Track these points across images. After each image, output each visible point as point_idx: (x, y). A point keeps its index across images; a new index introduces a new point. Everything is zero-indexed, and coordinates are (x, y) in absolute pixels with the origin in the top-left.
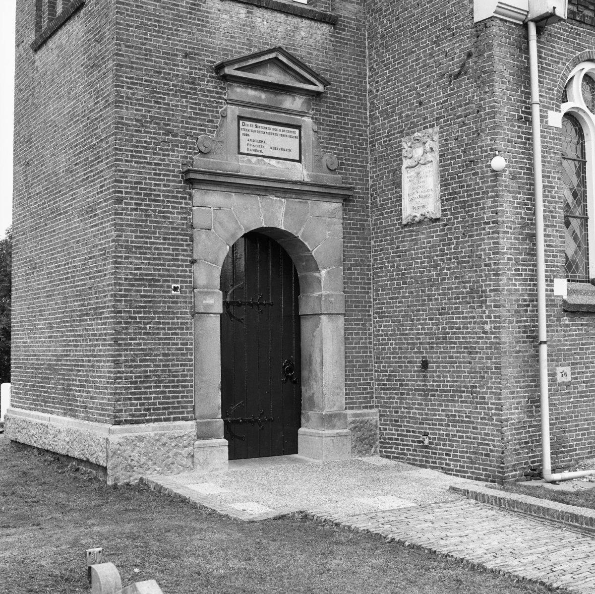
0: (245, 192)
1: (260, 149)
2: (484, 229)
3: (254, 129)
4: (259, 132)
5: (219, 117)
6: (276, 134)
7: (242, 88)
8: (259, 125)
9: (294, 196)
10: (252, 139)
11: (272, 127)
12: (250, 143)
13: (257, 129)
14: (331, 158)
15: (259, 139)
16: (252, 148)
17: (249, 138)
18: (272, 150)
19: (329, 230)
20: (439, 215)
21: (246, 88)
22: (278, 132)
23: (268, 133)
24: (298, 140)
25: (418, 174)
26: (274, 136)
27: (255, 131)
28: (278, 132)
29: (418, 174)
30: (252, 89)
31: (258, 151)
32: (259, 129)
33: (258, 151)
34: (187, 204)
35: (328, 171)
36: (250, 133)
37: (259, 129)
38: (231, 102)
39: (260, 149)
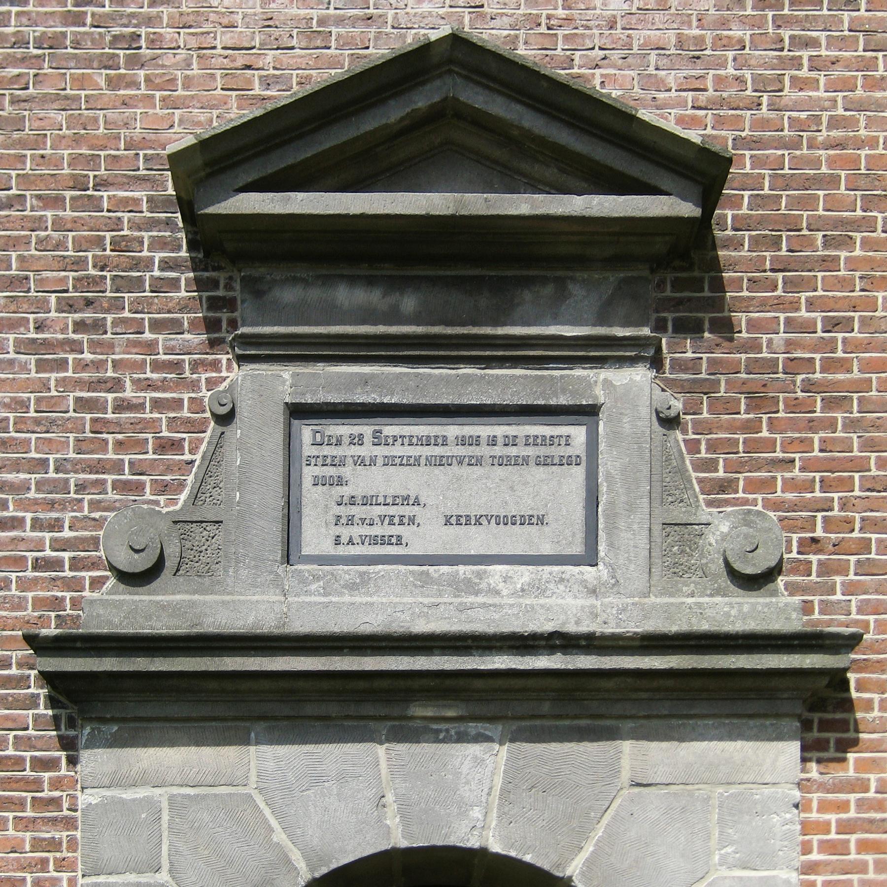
0: (310, 709)
1: (396, 530)
2: (116, 385)
3: (366, 450)
4: (389, 461)
5: (205, 421)
6: (477, 462)
7: (305, 282)
8: (391, 429)
9: (546, 707)
10: (359, 493)
11: (453, 430)
12: (342, 511)
13: (381, 451)
14: (748, 524)
15: (391, 492)
16: (357, 531)
17: (346, 491)
18: (453, 530)
19: (724, 842)
20: (303, 426)
21: (327, 280)
22: (484, 450)
23: (440, 462)
24: (579, 473)
25: (223, 433)
26: (465, 470)
27: (373, 461)
28: (484, 450)
29: (223, 433)
30: (352, 280)
31: (384, 540)
32: (398, 450)
33: (384, 540)
34: (56, 784)
35: (725, 581)
36: (346, 471)
37: (398, 450)
38: (654, 643)
39: (396, 530)
